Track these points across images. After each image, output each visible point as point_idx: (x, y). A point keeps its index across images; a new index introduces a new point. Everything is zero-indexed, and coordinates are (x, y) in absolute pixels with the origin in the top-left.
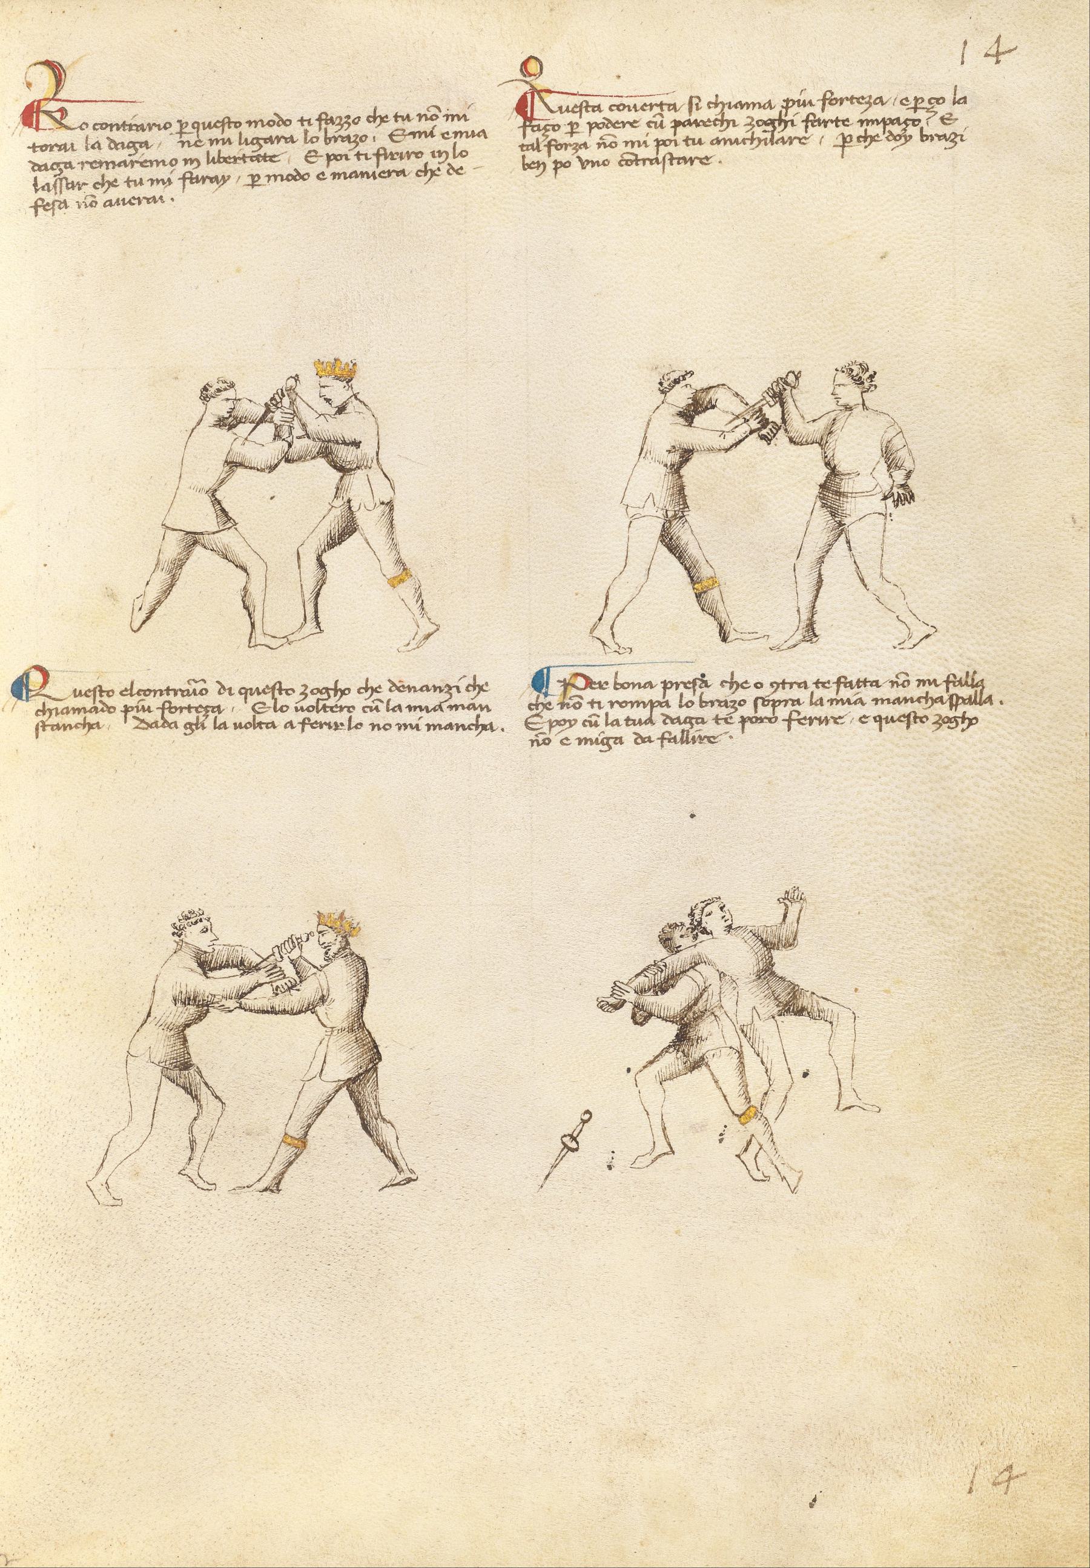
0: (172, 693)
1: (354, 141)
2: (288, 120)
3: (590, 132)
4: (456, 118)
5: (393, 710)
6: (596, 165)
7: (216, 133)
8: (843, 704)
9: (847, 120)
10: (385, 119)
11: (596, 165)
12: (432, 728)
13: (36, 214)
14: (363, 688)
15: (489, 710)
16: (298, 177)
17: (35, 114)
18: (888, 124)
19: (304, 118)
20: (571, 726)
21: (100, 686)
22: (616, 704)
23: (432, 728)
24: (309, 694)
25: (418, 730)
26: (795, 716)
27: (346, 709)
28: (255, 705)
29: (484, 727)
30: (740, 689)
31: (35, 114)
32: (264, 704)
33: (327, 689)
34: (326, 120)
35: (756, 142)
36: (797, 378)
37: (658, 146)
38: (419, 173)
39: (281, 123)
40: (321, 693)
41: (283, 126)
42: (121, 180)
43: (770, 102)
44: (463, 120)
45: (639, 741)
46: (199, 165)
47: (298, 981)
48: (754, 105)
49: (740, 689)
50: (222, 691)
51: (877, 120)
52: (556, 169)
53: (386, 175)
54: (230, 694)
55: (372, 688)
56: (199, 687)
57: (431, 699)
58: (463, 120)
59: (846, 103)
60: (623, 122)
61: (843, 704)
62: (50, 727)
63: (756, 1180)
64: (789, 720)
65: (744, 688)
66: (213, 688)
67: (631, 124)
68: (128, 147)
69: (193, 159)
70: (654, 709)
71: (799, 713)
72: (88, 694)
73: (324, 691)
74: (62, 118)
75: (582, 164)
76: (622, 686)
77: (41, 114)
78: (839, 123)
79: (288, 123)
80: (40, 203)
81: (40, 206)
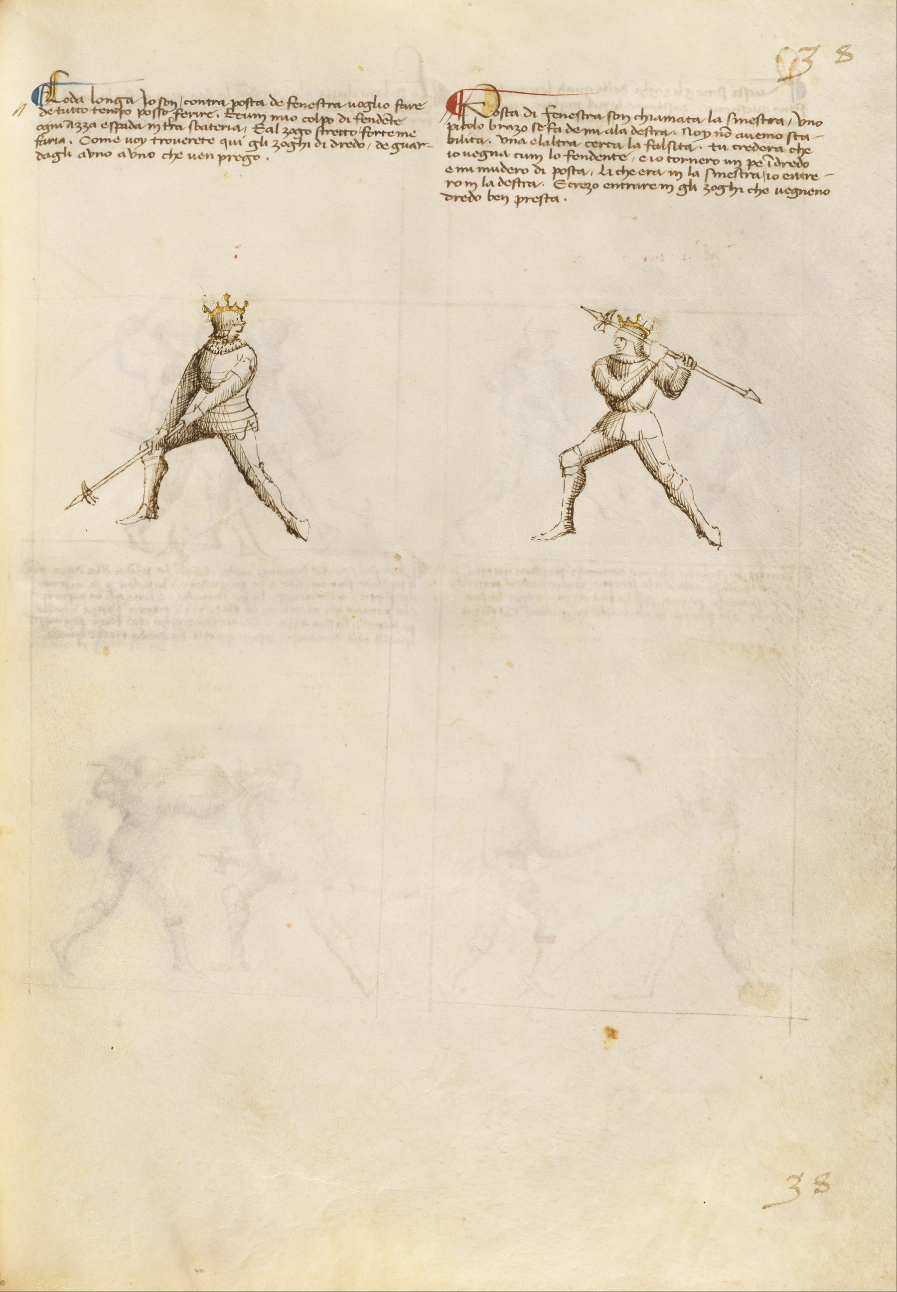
2: (128, 110)
3: (220, 163)
7: (233, 150)
9: (816, 176)
10: (807, 151)
12: (482, 170)
14: (621, 171)
15: (544, 173)
17: (458, 107)
18: (452, 130)
19: (715, 145)
20: (142, 143)
22: (710, 161)
23: (482, 170)
24: (592, 188)
25: (472, 171)
27: (810, 177)
29: (762, 191)
31: (458, 107)
34: (402, 105)
35: (626, 173)
37: (555, 173)
39: (356, 145)
40: (288, 146)
41: (357, 148)
44: (596, 133)
45: (379, 146)
49: (630, 175)
50: (318, 145)
58: (596, 133)
62: (692, 120)
64: (648, 145)
67: (209, 141)
69: (485, 168)
72: (731, 176)
74: (233, 111)
75: (502, 139)
76: (494, 197)
77: (797, 148)
78: (715, 148)
79: (284, 144)
81: (651, 145)
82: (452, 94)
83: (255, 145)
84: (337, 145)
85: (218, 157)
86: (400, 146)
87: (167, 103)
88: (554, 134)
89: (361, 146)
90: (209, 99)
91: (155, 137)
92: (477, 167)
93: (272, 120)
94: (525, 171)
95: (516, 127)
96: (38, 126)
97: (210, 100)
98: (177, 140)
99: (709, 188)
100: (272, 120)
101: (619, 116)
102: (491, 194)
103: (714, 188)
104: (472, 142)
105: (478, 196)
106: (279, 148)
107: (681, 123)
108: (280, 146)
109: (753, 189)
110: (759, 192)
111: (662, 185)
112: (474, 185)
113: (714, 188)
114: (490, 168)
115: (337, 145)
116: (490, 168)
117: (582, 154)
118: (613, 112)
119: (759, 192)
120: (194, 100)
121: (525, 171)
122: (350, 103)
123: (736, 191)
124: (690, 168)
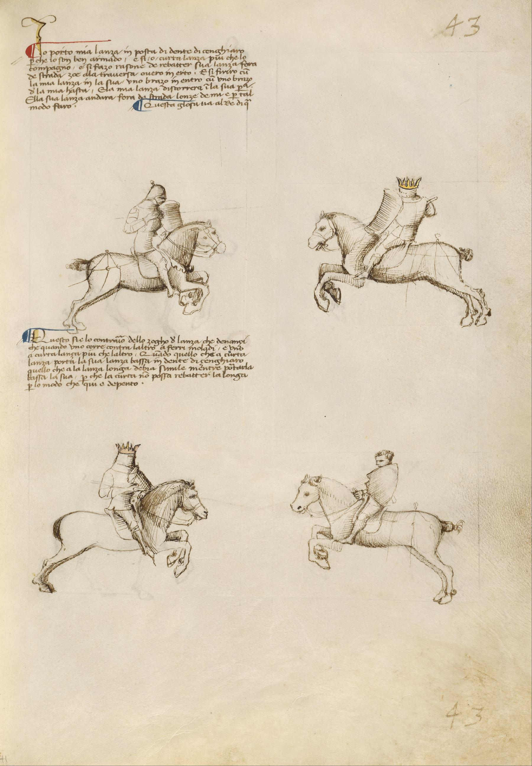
0: (147, 348)
1: (162, 83)
4: (53, 92)
5: (214, 88)
6: (175, 362)
8: (46, 85)
10: (45, 61)
11: (175, 362)
13: (119, 100)
16: (57, 385)
19: (67, 51)
21: (63, 338)
24: (108, 69)
26: (219, 70)
27: (163, 65)
28: (99, 89)
30: (98, 378)
32: (103, 88)
33: (158, 341)
36: (144, 355)
38: (37, 61)
42: (97, 354)
43: (57, 98)
46: (178, 83)
47: (36, 44)
48: (38, 363)
50: (239, 104)
51: (138, 66)
52: (153, 378)
53: (194, 88)
54: (200, 53)
55: (59, 369)
56: (121, 339)
57: (109, 56)
59: (185, 89)
60: (186, 80)
61: (46, 85)
62: (74, 354)
63: (22, 21)
65: (99, 377)
66: (127, 339)
68: (120, 369)
70: (154, 379)
71: (220, 69)
73: (157, 342)
76: (78, 60)
79: (48, 107)
80: (57, 105)
81: (170, 347)
82: (25, 331)
83: (122, 369)
84: (65, 60)
85: (28, 386)
86: (124, 369)
87: (64, 60)
88: (234, 74)
89: (235, 72)
90: (210, 56)
91: (120, 346)
92: (49, 51)
93: (167, 75)
94: (69, 107)
95: (121, 361)
96: (68, 383)
97: (198, 374)
98: (48, 347)
99: (71, 75)
100: (167, 75)
101: (65, 60)
102: (43, 350)
103: (74, 75)
104: (192, 81)
105: (35, 68)
106: (71, 77)
107: (232, 88)
108: (72, 76)
109: (102, 353)
110: (59, 371)
111: (191, 367)
112: (69, 60)
113: (74, 75)
114: (55, 90)
115: (197, 51)
116: (55, 90)
117: (238, 77)
118: (129, 65)
119: (59, 371)
120: (58, 51)
121: (70, 53)
122: (86, 92)
123: (225, 52)
124: (137, 86)
